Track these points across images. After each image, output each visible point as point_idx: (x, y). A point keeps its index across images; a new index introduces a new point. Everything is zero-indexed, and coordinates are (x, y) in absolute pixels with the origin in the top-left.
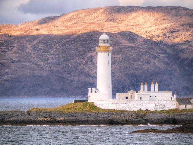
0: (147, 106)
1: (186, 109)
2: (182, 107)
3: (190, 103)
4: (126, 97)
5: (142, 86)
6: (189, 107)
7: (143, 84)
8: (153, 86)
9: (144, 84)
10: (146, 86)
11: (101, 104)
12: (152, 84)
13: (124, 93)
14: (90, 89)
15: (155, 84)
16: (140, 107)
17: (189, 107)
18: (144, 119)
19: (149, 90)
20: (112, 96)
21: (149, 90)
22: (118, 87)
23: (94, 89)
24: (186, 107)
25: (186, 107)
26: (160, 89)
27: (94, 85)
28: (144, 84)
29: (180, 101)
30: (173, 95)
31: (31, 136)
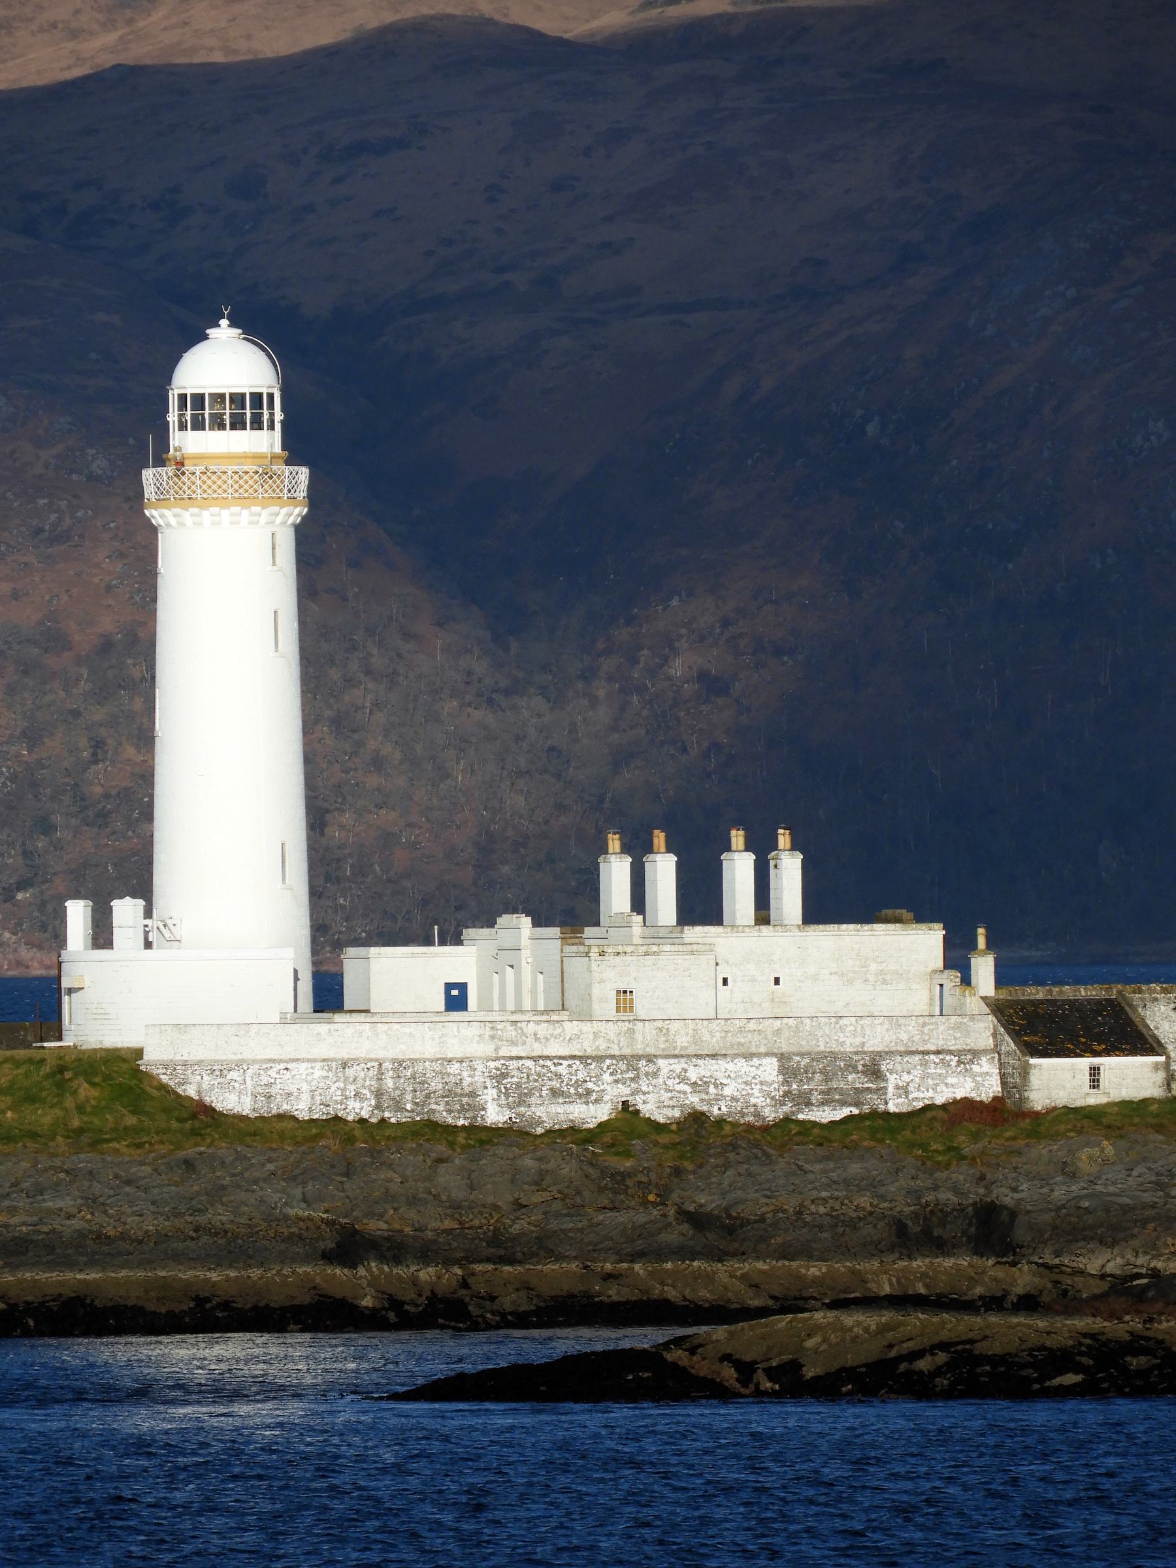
0: (693, 1075)
1: (1095, 1099)
2: (1059, 1081)
3: (1135, 1040)
4: (449, 986)
5: (616, 872)
6: (1129, 1077)
7: (626, 849)
8: (739, 868)
9: (638, 850)
10: (663, 869)
11: (219, 1069)
12: (728, 848)
13: (431, 948)
14: (77, 915)
15: (638, 849)
16: (624, 1091)
17: (1129, 1077)
18: (686, 1216)
19: (701, 903)
20: (342, 975)
21: (701, 903)
22: (371, 885)
23: (126, 910)
24: (1095, 1083)
25: (1095, 1083)
26: (821, 908)
27: (124, 866)
28: (638, 850)
29: (1038, 1029)
30: (957, 958)
31: (907, 1548)
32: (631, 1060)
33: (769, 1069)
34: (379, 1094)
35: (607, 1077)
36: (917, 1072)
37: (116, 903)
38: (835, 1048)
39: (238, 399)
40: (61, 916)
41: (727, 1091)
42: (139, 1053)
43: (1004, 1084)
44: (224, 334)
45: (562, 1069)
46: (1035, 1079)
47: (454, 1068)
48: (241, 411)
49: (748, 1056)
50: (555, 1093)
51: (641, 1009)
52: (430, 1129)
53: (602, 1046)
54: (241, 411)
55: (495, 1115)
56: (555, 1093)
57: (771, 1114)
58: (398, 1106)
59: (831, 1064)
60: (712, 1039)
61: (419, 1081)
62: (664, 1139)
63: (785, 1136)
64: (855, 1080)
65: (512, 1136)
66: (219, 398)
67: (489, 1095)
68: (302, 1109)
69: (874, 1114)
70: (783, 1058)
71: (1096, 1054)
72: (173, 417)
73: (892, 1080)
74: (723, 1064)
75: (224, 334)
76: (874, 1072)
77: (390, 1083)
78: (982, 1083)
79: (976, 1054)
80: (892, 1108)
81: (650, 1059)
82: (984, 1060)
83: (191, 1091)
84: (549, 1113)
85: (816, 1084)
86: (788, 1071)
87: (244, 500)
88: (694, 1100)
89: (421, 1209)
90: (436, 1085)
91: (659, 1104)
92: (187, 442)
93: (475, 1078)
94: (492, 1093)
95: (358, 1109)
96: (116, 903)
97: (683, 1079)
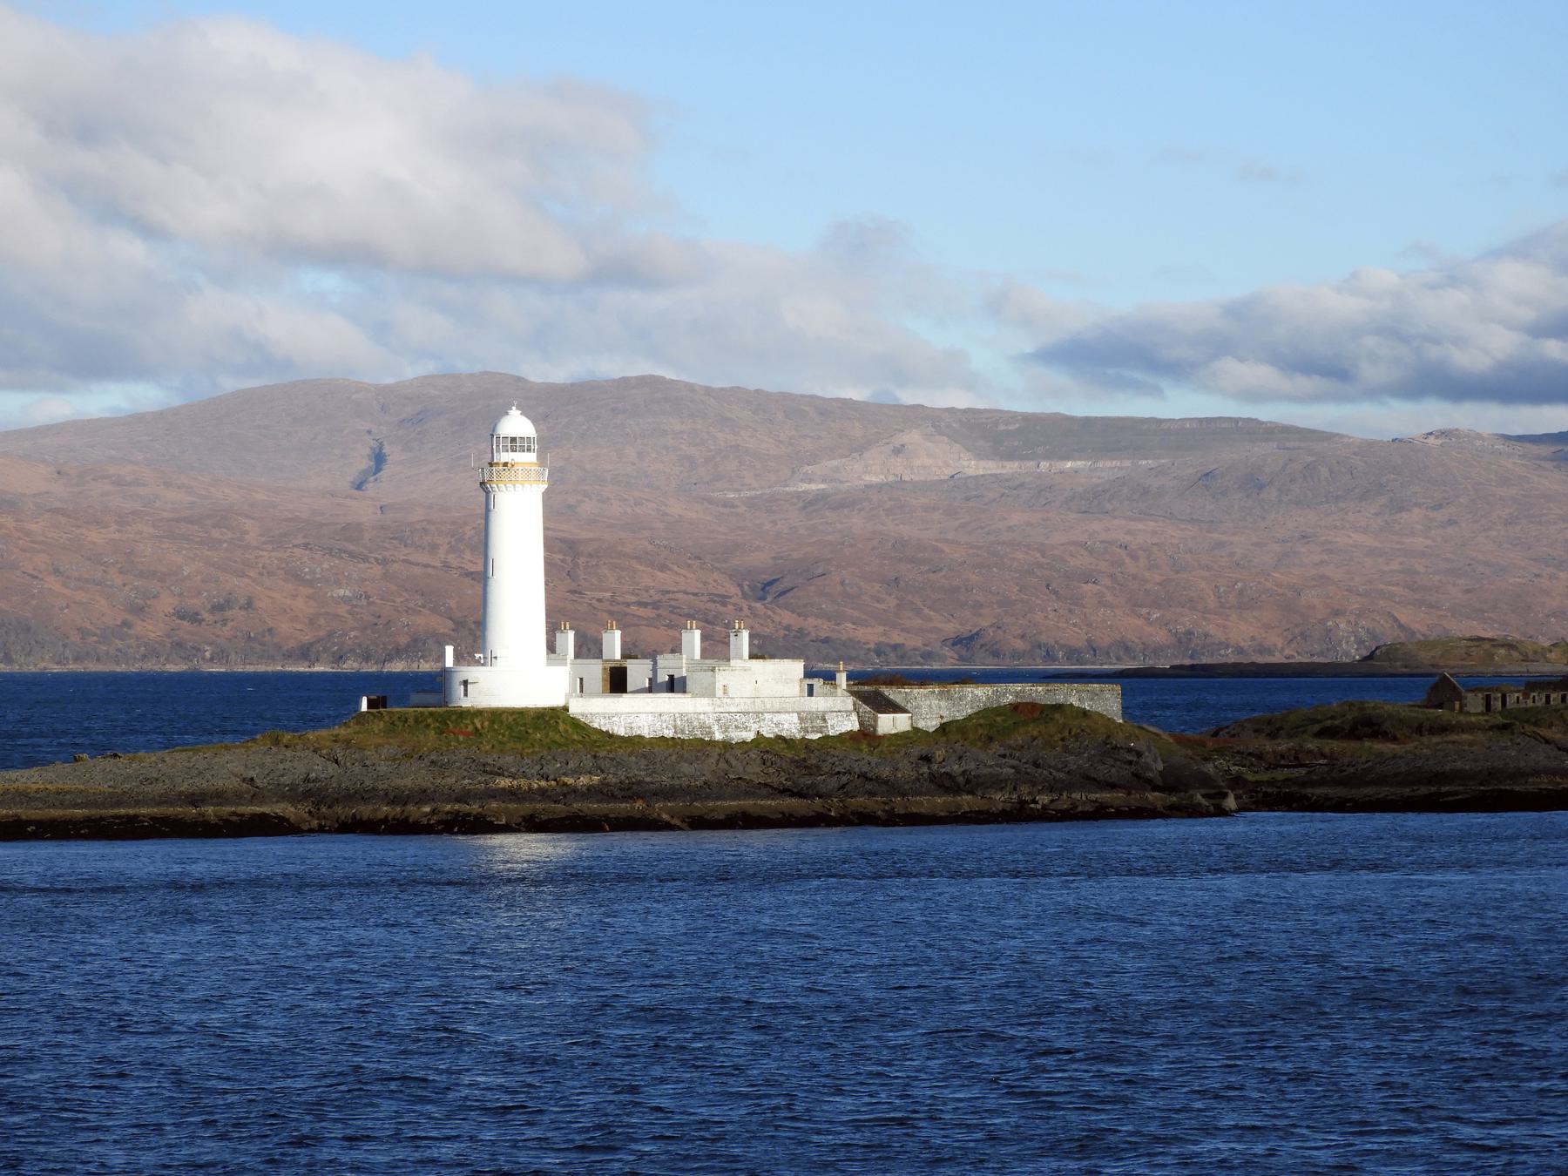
11: (610, 717)
29: (962, 659)
32: (757, 713)
33: (795, 718)
42: (566, 709)
43: (861, 723)
44: (515, 413)
55: (718, 736)
57: (798, 736)
58: (683, 732)
60: (777, 707)
61: (690, 722)
64: (819, 723)
65: (726, 745)
67: (715, 728)
68: (646, 733)
73: (830, 723)
75: (515, 413)
78: (852, 724)
83: (596, 725)
84: (737, 736)
89: (981, 641)
95: (669, 733)
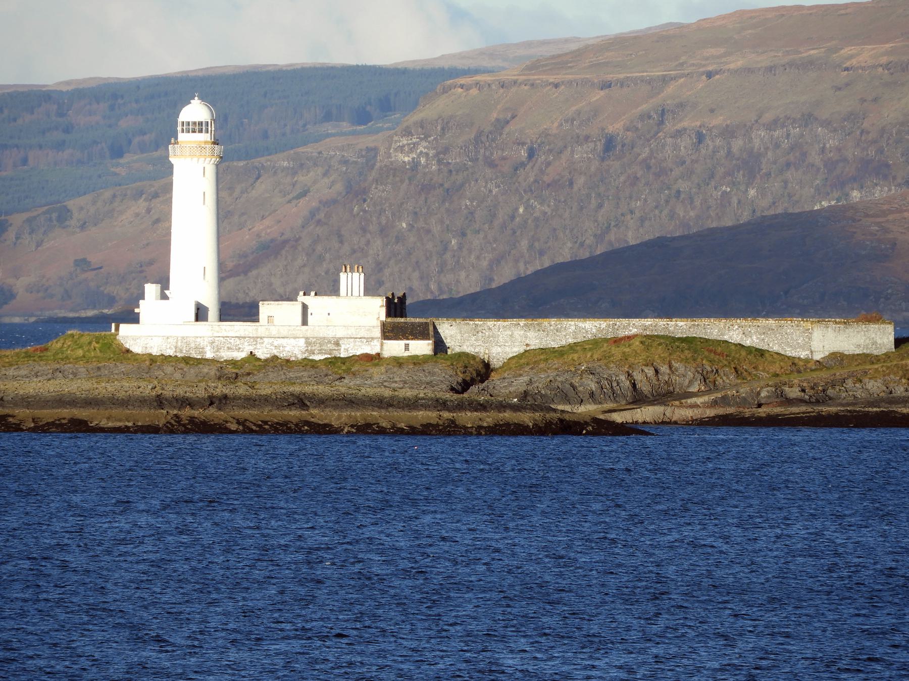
0: (276, 343)
1: (407, 354)
2: (395, 348)
16: (251, 348)
32: (255, 339)
33: (302, 342)
34: (176, 347)
35: (246, 344)
36: (352, 344)
37: (146, 285)
38: (326, 335)
39: (201, 123)
40: (873, 318)
41: (287, 349)
45: (232, 341)
46: (385, 347)
47: (198, 340)
48: (198, 127)
49: (295, 338)
50: (229, 348)
51: (276, 323)
52: (187, 360)
53: (247, 334)
54: (198, 127)
55: (209, 355)
56: (229, 348)
58: (181, 351)
59: (323, 341)
61: (188, 344)
62: (257, 363)
63: (308, 364)
66: (195, 123)
69: (335, 358)
70: (307, 338)
71: (408, 339)
72: (179, 128)
73: (343, 347)
74: (286, 340)
76: (337, 344)
77: (179, 344)
78: (372, 349)
79: (373, 338)
80: (342, 356)
81: (261, 338)
82: (375, 341)
84: (226, 355)
85: (317, 347)
86: (308, 343)
87: (192, 155)
88: (275, 352)
90: (193, 345)
91: (262, 353)
92: (182, 137)
93: (204, 343)
94: (209, 348)
96: (146, 285)
97: (272, 345)
